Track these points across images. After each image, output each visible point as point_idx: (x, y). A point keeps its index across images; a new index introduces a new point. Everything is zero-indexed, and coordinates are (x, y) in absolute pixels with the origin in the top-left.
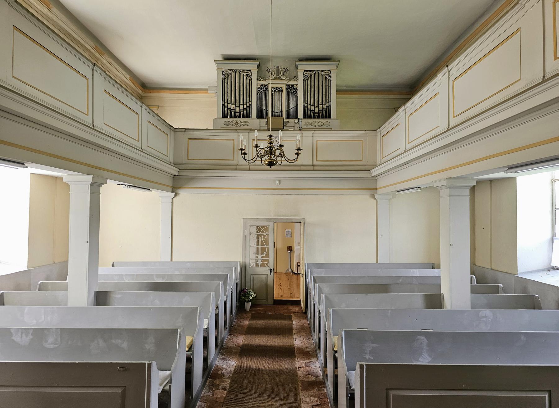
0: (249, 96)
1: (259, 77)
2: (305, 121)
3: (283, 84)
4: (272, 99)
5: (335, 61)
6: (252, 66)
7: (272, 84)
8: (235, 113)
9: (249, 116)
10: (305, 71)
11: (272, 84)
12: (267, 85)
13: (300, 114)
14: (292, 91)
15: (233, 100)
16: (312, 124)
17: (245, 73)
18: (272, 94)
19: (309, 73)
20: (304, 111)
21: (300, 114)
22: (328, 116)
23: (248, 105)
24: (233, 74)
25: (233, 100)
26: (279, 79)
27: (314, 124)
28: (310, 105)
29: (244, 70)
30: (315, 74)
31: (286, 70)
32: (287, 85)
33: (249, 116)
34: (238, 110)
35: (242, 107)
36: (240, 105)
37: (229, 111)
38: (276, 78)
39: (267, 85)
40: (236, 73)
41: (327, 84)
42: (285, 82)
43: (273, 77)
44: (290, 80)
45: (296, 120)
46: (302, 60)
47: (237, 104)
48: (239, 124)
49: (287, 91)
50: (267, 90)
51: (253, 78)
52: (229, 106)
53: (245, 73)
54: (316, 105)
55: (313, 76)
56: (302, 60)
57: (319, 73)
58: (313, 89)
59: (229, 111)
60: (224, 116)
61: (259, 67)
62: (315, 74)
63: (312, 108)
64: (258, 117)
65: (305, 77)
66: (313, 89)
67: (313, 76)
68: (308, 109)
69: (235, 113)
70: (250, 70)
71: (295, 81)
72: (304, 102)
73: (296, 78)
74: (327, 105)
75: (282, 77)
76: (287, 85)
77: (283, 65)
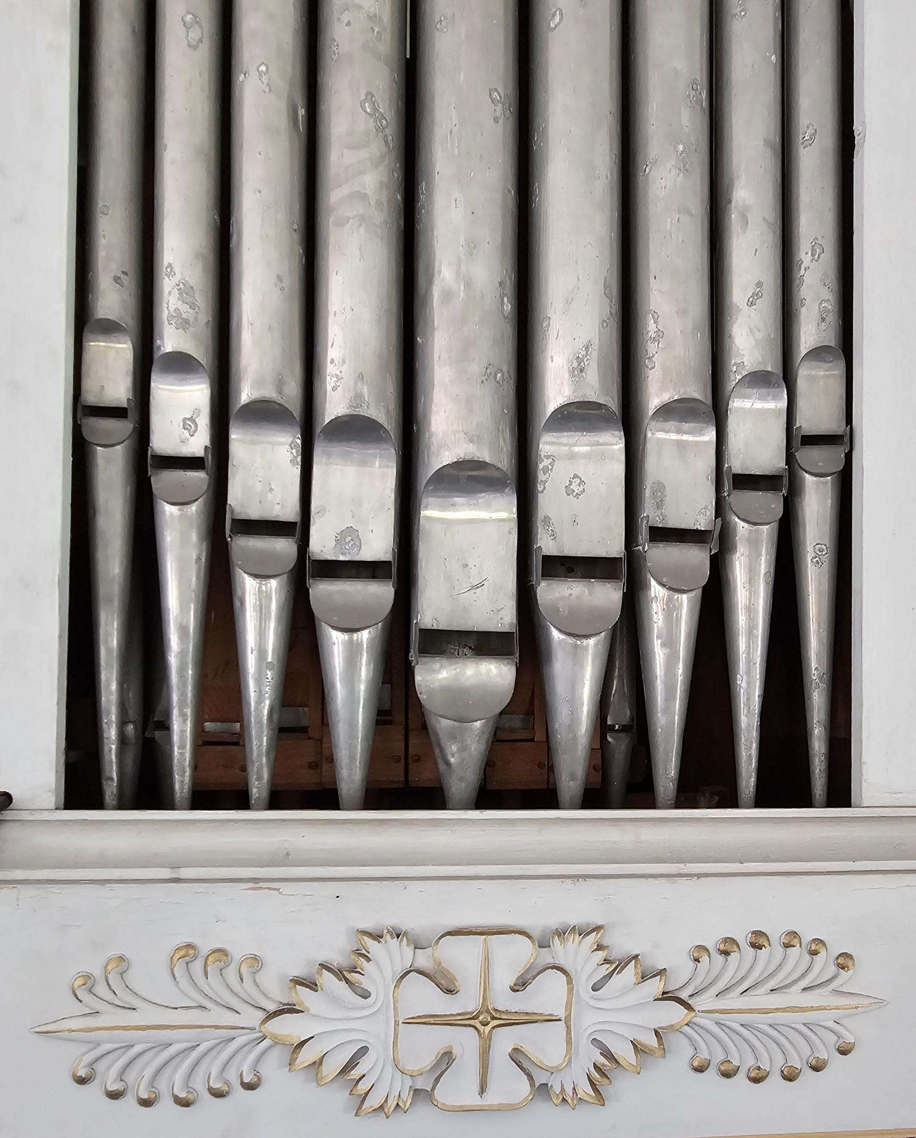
8: (402, 643)
16: (329, 1022)
34: (468, 561)
37: (260, 607)
47: (460, 420)
54: (460, 420)
59: (260, 607)
63: (354, 504)
68: (221, 531)
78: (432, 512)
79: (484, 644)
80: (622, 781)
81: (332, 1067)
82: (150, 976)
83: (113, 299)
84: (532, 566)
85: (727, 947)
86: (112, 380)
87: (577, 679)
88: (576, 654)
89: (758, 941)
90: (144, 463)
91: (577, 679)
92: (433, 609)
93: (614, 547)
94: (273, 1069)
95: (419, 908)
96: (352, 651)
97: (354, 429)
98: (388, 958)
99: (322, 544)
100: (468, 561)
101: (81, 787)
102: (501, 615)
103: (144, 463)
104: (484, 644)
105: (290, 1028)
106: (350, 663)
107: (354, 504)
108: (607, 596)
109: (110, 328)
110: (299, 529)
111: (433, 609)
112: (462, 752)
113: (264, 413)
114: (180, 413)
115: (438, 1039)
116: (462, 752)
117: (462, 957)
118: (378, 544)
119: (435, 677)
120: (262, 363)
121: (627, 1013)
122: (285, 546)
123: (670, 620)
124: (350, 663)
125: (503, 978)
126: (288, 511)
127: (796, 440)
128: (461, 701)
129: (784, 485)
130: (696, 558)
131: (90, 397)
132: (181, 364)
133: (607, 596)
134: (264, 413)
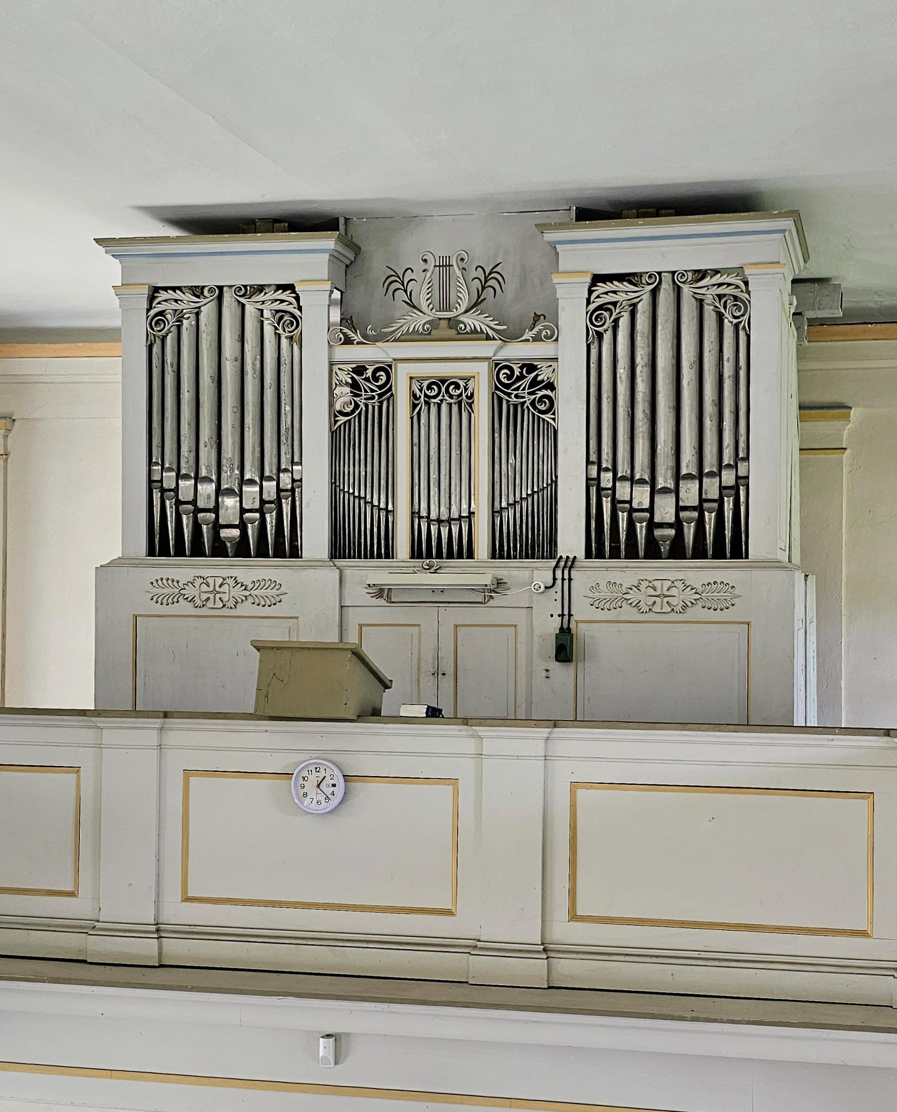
0: (289, 437)
1: (351, 326)
2: (596, 578)
3: (472, 363)
4: (414, 445)
5: (781, 215)
6: (307, 262)
7: (412, 363)
8: (652, 525)
9: (286, 547)
10: (598, 279)
11: (412, 363)
12: (387, 369)
13: (571, 538)
14: (523, 396)
15: (207, 455)
16: (634, 596)
17: (269, 303)
18: (415, 419)
19: (624, 292)
20: (593, 518)
21: (571, 538)
22: (730, 544)
23: (286, 480)
24: (208, 311)
25: (207, 455)
26: (456, 331)
27: (642, 596)
28: (632, 480)
29: (261, 289)
30: (654, 293)
31: (490, 277)
32: (498, 366)
33: (286, 547)
34: (665, 510)
35: (690, 493)
36: (242, 481)
37: (623, 517)
38: (434, 324)
39: (387, 369)
40: (220, 298)
41: (728, 352)
42: (487, 349)
43: (418, 321)
44: (509, 336)
45: (540, 572)
46: (588, 213)
47: (664, 480)
48: (230, 593)
49: (497, 402)
50: (387, 391)
51: (306, 326)
52: (623, 491)
53: (269, 303)
54: (664, 480)
55: (643, 308)
56: (588, 213)
57: (678, 291)
58: (642, 387)
59: (623, 517)
60: (160, 543)
61: (349, 266)
62: (654, 293)
63: (642, 496)
64: (341, 547)
65: (596, 315)
66: (642, 387)
67: (643, 308)
68: (614, 502)
69: (217, 526)
70: (290, 287)
71: (537, 339)
72: (593, 460)
73: (543, 323)
74: (728, 478)
75: (471, 321)
76: (498, 366)
77: (479, 244)
78: (657, 499)
79: (670, 526)
80: (699, 553)
81: (634, 604)
82: (603, 587)
83: (593, 457)
84: (679, 509)
85: (709, 584)
86: (594, 473)
87: (689, 532)
88: (689, 528)
89: (715, 583)
90: (599, 489)
91: (689, 532)
92: (603, 485)
93: (696, 503)
94: (700, 590)
95: (205, 573)
96: (641, 527)
97: (642, 481)
98: (644, 584)
99: (635, 505)
100: (665, 510)
101: (588, 555)
102: (672, 519)
103: (599, 489)
104: (670, 526)
105: (626, 596)
106: (641, 530)
107: (642, 496)
108: (695, 514)
109: (593, 463)
110: (630, 502)
111: (603, 485)
112: (664, 548)
113: (623, 478)
114: (607, 479)
115: (654, 599)
116: (664, 548)
117: (658, 584)
118: (646, 504)
119: (658, 533)
120: (623, 469)
121: (689, 596)
122: (627, 506)
123: (710, 518)
124: (641, 530)
125: (665, 588)
126: (628, 499)
127: (738, 478)
128: (664, 538)
129: (736, 488)
130: (715, 505)
131: (589, 477)
132: (607, 470)
133: (695, 514)
134: (623, 478)
